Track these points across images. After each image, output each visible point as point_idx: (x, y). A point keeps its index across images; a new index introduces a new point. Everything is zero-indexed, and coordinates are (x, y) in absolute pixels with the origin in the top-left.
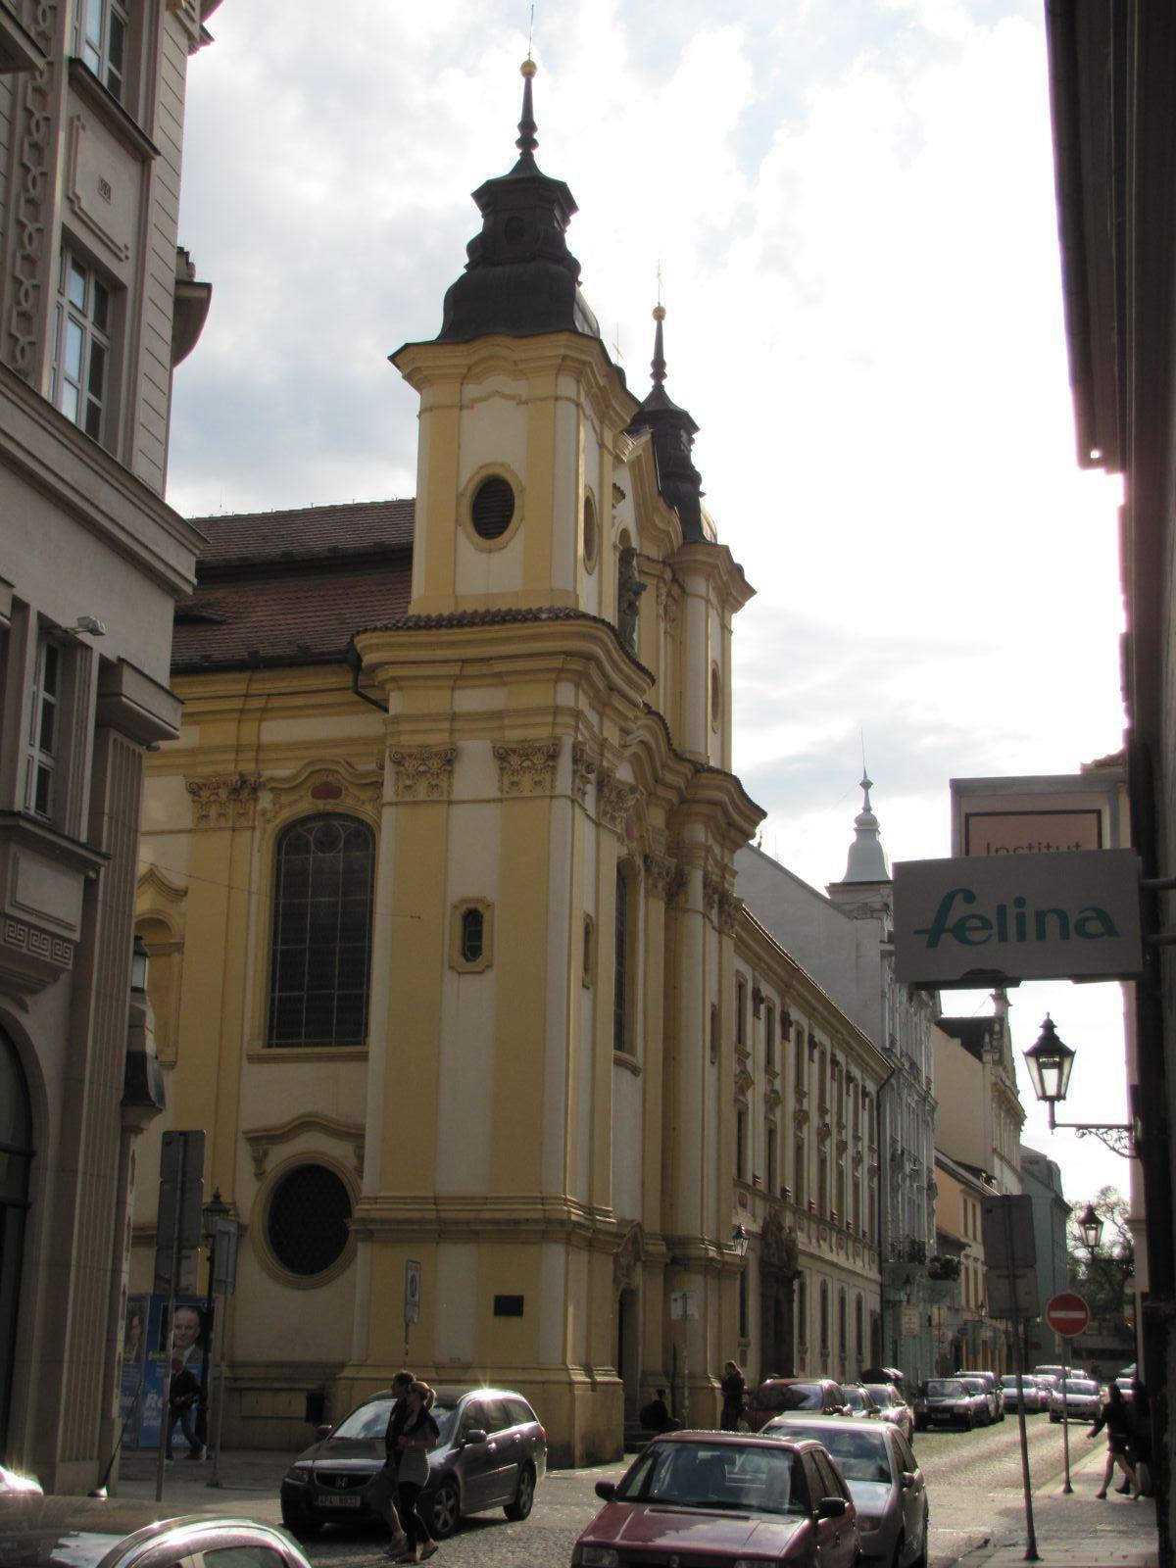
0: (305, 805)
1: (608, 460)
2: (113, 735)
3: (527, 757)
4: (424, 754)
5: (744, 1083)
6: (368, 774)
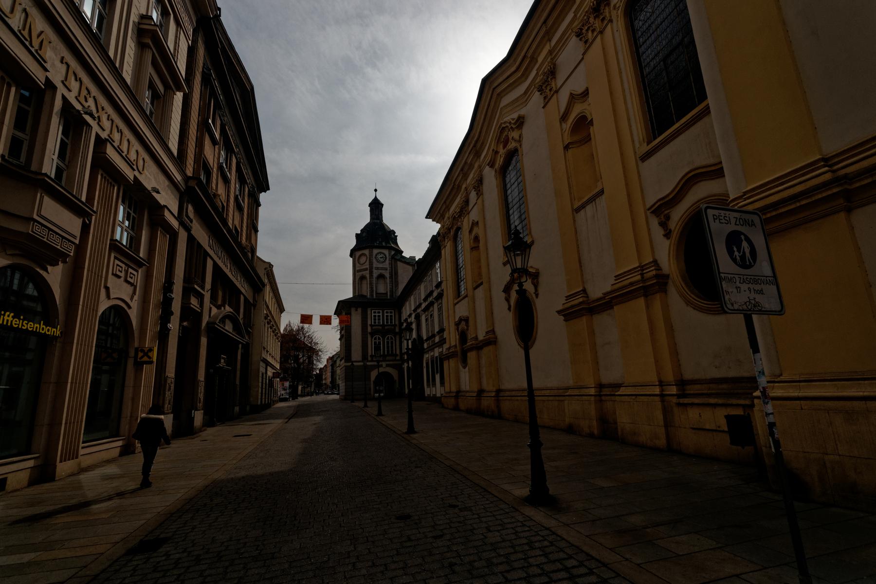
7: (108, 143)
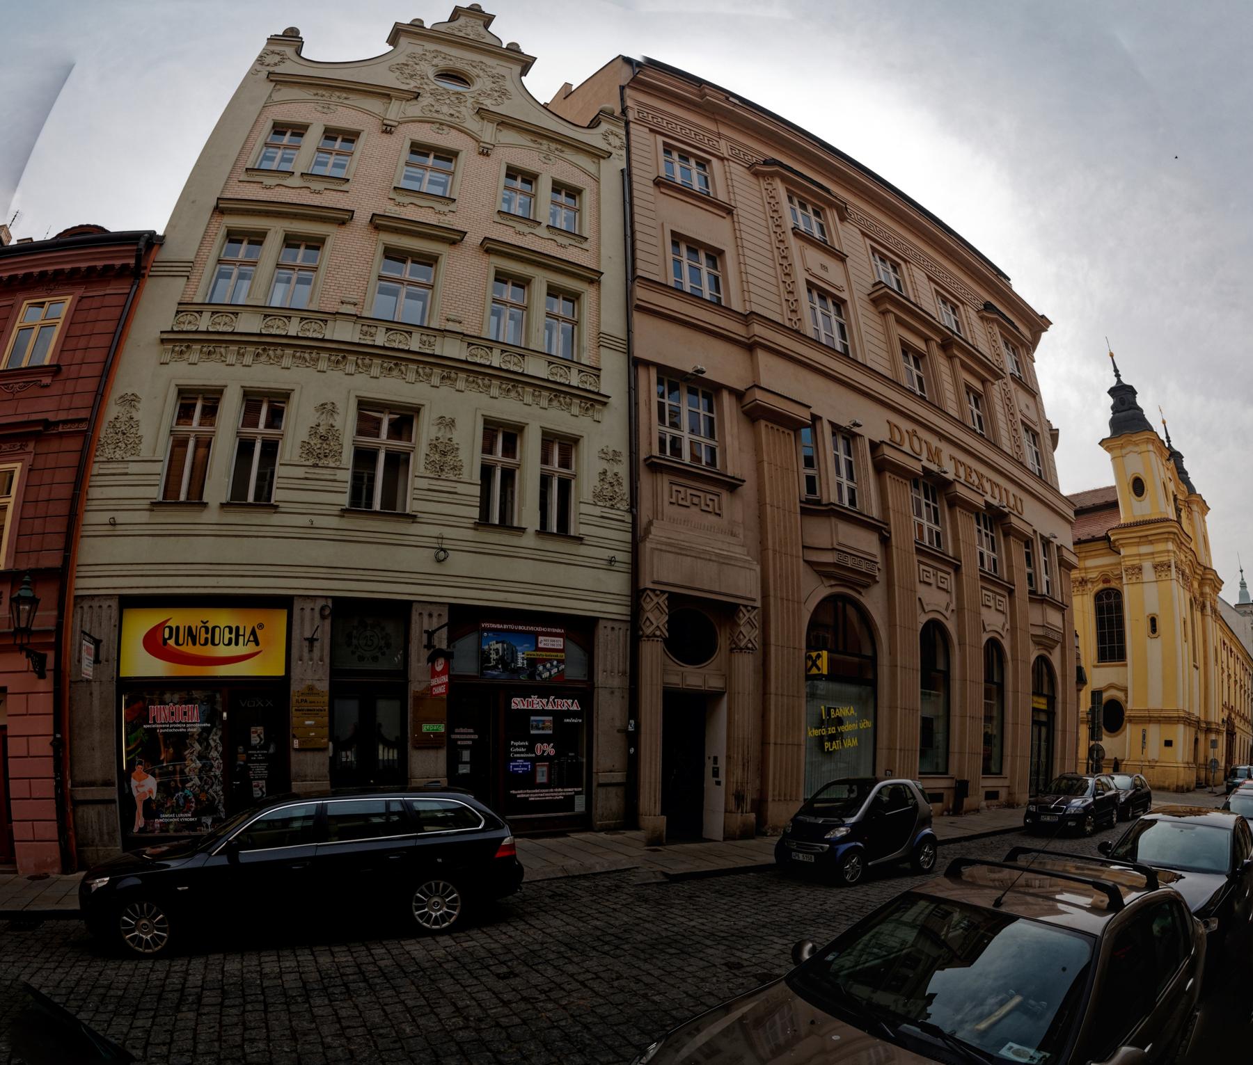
0: (1101, 586)
2: (1062, 568)
4: (1133, 567)
5: (1223, 672)
6: (1118, 575)
7: (956, 483)
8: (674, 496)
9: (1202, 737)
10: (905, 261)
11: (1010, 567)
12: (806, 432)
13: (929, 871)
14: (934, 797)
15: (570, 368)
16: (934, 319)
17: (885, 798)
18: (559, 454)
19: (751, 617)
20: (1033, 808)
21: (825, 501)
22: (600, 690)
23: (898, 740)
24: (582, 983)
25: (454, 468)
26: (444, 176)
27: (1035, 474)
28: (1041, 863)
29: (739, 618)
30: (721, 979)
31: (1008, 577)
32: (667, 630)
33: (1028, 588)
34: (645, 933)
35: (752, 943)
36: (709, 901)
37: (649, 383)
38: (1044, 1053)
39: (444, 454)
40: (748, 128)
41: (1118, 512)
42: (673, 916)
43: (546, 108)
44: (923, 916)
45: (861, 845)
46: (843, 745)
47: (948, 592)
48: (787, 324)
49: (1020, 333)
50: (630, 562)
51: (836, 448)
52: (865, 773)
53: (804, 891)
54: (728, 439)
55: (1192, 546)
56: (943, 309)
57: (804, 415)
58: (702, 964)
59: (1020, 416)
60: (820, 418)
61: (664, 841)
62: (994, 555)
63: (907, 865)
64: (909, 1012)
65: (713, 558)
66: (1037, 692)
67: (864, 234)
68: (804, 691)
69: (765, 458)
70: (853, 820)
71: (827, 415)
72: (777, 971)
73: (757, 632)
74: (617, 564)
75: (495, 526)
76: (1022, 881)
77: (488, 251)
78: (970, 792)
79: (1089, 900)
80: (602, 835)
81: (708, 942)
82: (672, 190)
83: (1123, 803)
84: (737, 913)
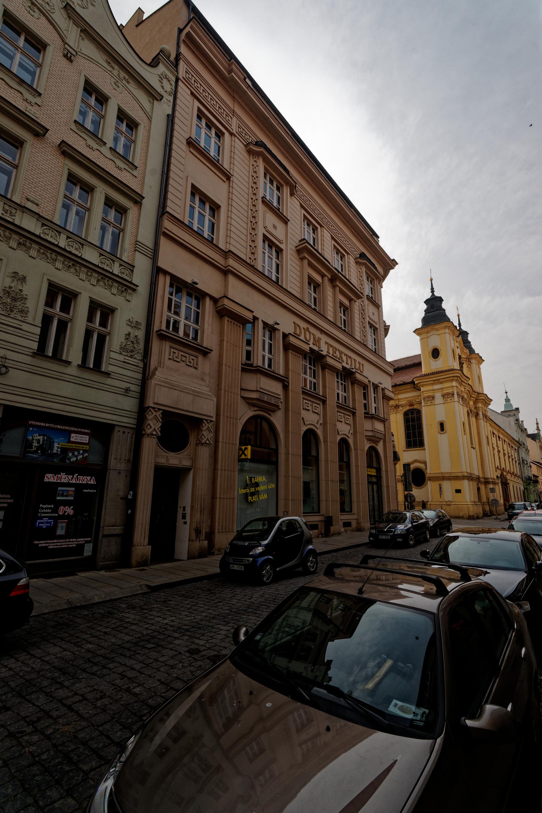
0: (408, 408)
1: (455, 342)
2: (384, 400)
3: (448, 395)
4: (429, 397)
7: (327, 357)
8: (171, 355)
9: (482, 487)
10: (321, 226)
11: (354, 400)
12: (249, 326)
13: (314, 573)
14: (313, 527)
15: (114, 261)
16: (329, 263)
17: (284, 528)
18: (100, 317)
19: (209, 426)
20: (373, 531)
21: (255, 365)
22: (111, 471)
23: (290, 495)
24: (70, 708)
25: (21, 311)
26: (33, 65)
27: (373, 351)
28: (383, 564)
29: (202, 426)
30: (186, 665)
31: (352, 406)
32: (160, 432)
33: (364, 411)
34: (131, 634)
35: (206, 631)
36: (177, 603)
37: (165, 285)
38: (424, 710)
39: (14, 299)
40: (252, 111)
41: (421, 368)
42: (152, 617)
43: (121, 31)
44: (314, 603)
45: (272, 558)
46: (259, 498)
47: (318, 414)
48: (248, 261)
49: (377, 271)
50: (139, 391)
51: (264, 336)
52: (272, 514)
53: (238, 591)
54: (206, 326)
55: (470, 382)
56: (336, 257)
57: (249, 316)
58: (172, 653)
59: (368, 319)
60: (258, 319)
61: (149, 563)
62: (345, 394)
63: (300, 569)
64: (316, 677)
65: (190, 392)
66: (370, 466)
67: (302, 206)
68: (237, 468)
69: (225, 339)
70: (266, 542)
71: (262, 317)
72: (224, 652)
73: (212, 435)
74: (130, 392)
75: (49, 357)
76: (373, 576)
77: (64, 154)
78: (334, 523)
79: (422, 589)
80: (103, 573)
81: (176, 635)
82: (197, 152)
83: (431, 527)
84: (196, 610)
